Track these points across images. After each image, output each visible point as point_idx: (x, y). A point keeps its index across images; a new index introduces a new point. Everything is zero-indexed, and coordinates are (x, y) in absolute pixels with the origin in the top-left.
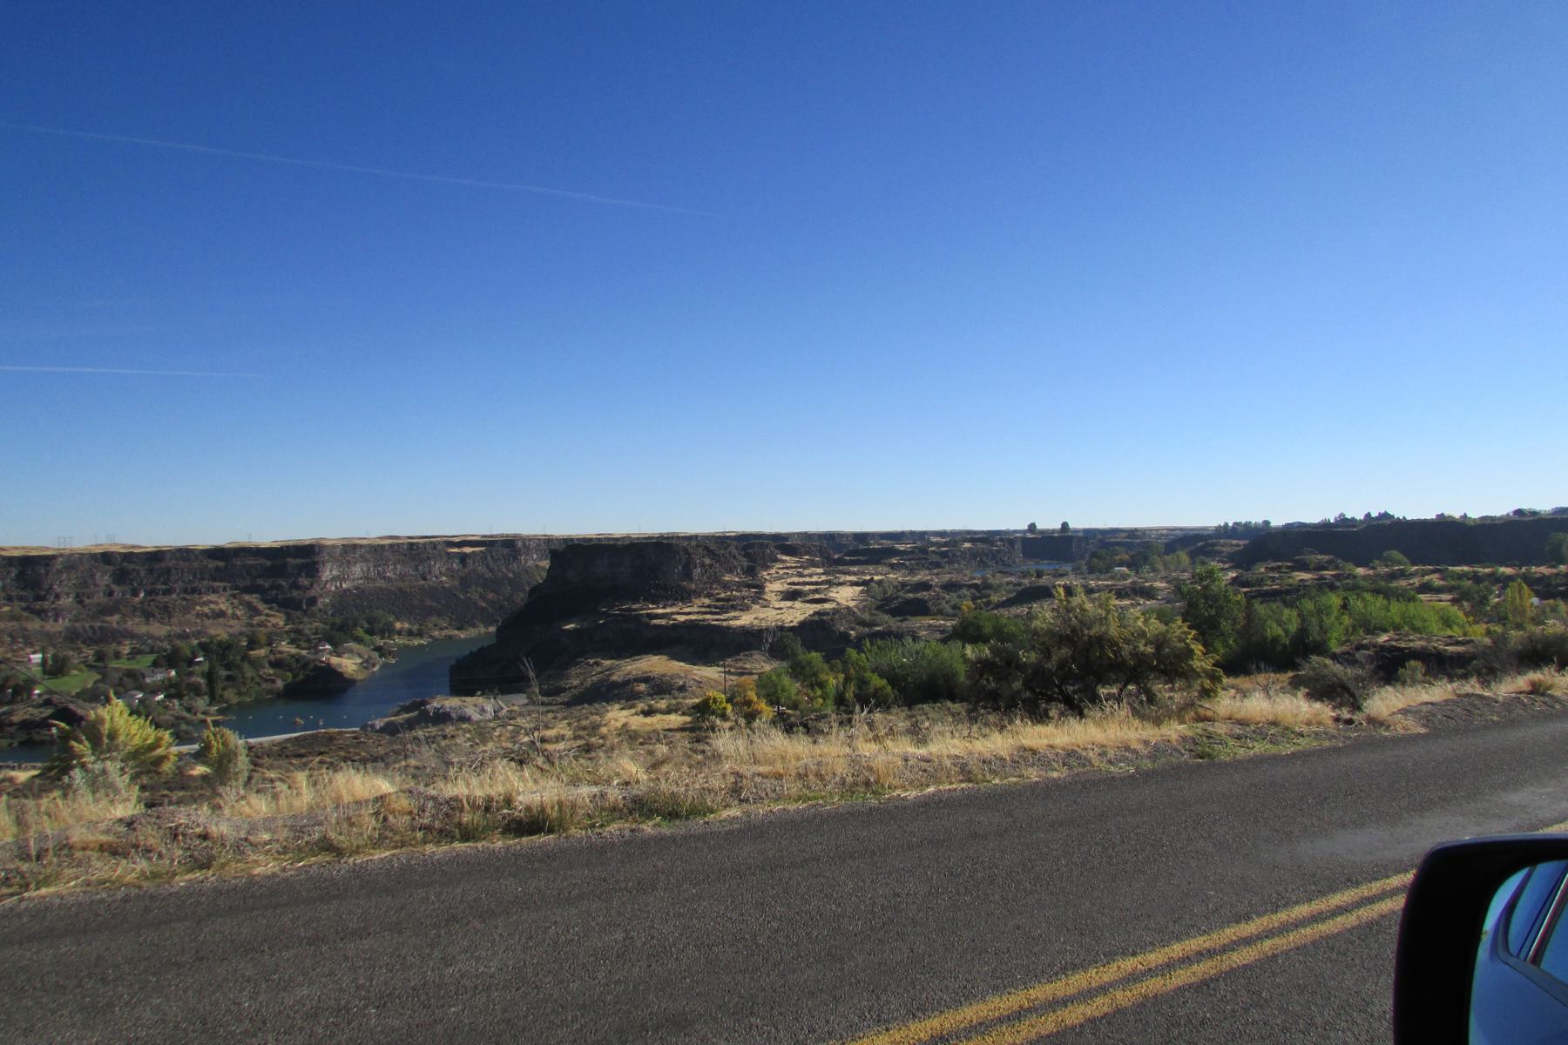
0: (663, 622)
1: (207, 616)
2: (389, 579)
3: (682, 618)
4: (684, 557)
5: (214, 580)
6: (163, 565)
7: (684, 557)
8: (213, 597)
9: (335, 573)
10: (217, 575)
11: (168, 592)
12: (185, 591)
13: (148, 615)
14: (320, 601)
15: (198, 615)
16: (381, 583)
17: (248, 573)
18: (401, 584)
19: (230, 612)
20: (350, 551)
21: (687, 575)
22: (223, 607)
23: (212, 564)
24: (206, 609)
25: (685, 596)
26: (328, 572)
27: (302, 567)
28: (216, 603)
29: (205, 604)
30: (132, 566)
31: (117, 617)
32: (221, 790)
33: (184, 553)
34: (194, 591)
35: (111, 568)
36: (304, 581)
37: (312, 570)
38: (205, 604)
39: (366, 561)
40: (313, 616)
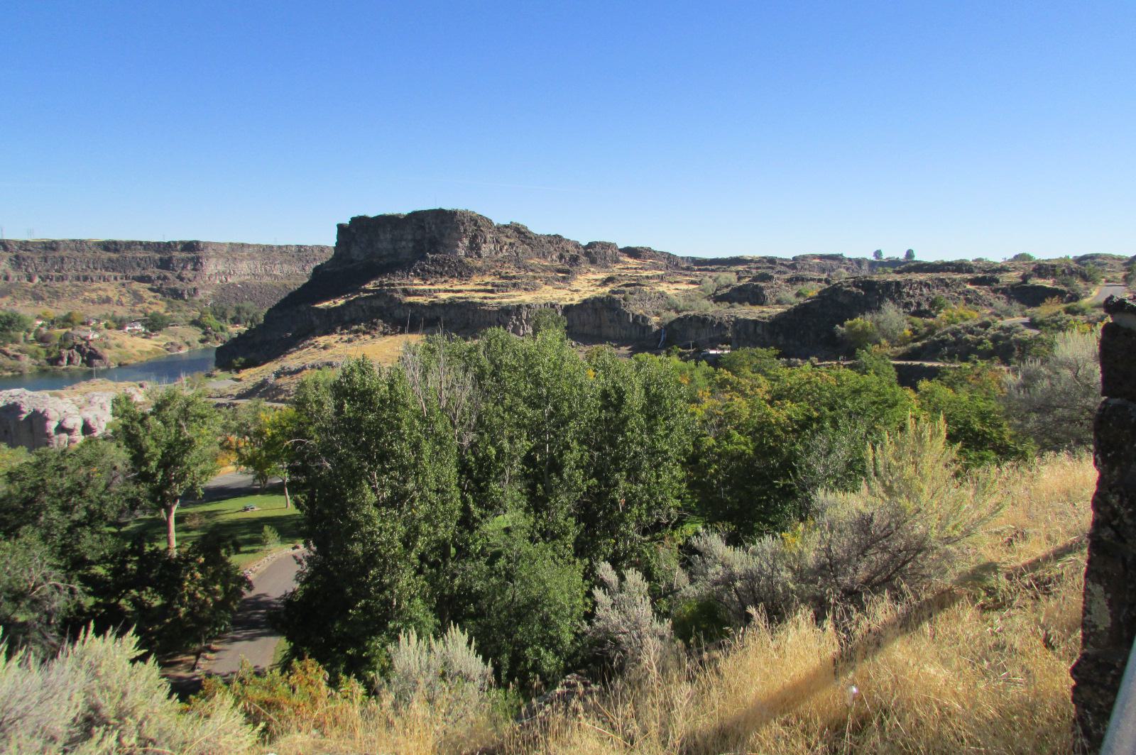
0: (420, 300)
1: (93, 302)
2: (276, 277)
3: (444, 296)
4: (471, 228)
5: (107, 269)
6: (57, 254)
7: (471, 228)
8: (103, 285)
9: (221, 268)
10: (111, 266)
11: (62, 279)
12: (78, 279)
13: (37, 298)
14: (200, 292)
15: (85, 300)
16: (266, 280)
17: (139, 265)
18: (286, 282)
19: (116, 298)
20: (236, 250)
21: (474, 248)
22: (110, 294)
23: (106, 255)
24: (94, 296)
25: (463, 272)
26: (212, 267)
27: (186, 261)
28: (105, 290)
29: (94, 290)
30: (28, 253)
31: (8, 299)
32: (710, 318)
33: (79, 245)
34: (86, 279)
35: (9, 254)
36: (188, 274)
37: (197, 263)
38: (94, 290)
39: (253, 258)
40: (193, 305)
